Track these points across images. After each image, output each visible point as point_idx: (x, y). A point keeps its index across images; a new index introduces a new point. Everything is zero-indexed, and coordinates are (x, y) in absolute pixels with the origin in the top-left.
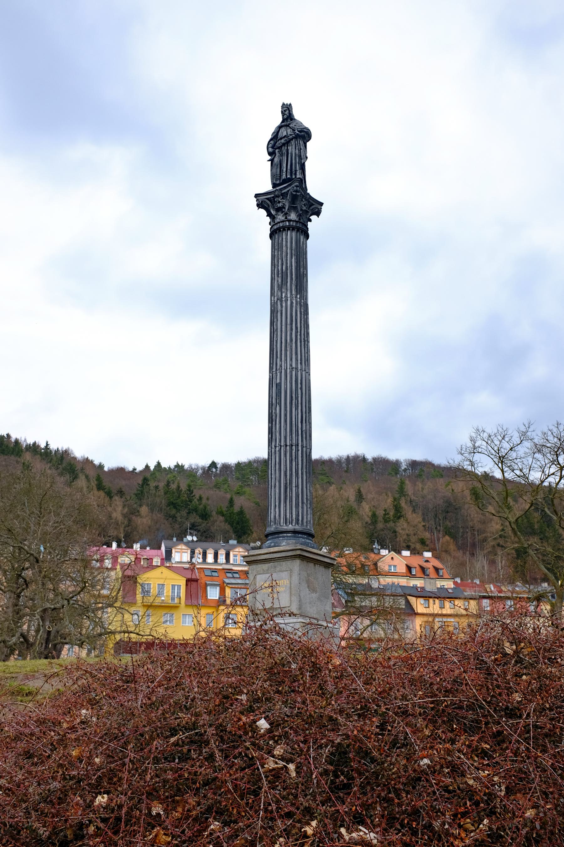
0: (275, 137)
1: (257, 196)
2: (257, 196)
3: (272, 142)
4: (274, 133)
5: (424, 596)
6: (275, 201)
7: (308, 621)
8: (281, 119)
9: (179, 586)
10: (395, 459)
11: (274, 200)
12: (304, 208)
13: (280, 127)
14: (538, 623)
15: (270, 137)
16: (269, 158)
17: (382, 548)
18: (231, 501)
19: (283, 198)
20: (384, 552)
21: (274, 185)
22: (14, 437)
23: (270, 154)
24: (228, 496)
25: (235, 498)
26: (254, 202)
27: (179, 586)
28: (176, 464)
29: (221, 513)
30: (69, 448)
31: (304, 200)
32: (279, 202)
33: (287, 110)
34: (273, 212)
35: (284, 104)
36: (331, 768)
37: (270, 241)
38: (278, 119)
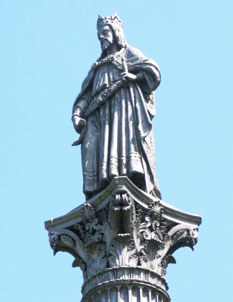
0: (89, 88)
1: (49, 225)
2: (49, 225)
3: (82, 104)
4: (85, 81)
5: (152, 170)
6: (86, 232)
7: (111, 287)
8: (100, 52)
11: (84, 228)
12: (151, 236)
13: (96, 70)
15: (78, 90)
19: (100, 223)
23: (79, 128)
26: (44, 237)
31: (147, 219)
32: (94, 232)
33: (193, 249)
34: (82, 254)
35: (176, 263)
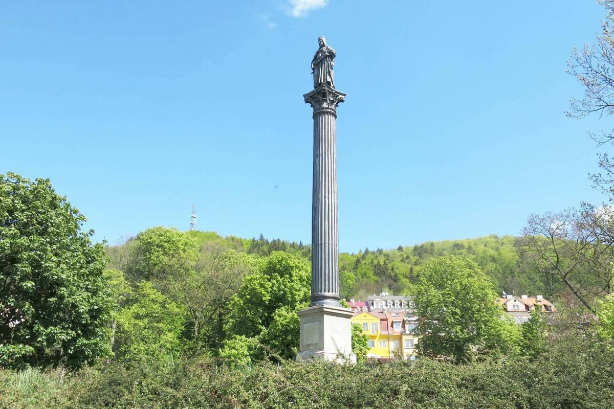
0: (316, 58)
9: (376, 324)
10: (239, 238)
14: (2, 241)
16: (312, 71)
17: (508, 294)
18: (411, 270)
20: (509, 297)
21: (315, 88)
22: (281, 240)
23: (313, 69)
24: (410, 266)
25: (414, 267)
27: (376, 324)
28: (377, 249)
29: (406, 277)
30: (416, 246)
32: (316, 98)
36: (88, 273)
37: (312, 120)
38: (317, 48)
